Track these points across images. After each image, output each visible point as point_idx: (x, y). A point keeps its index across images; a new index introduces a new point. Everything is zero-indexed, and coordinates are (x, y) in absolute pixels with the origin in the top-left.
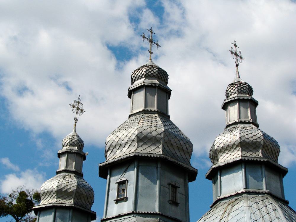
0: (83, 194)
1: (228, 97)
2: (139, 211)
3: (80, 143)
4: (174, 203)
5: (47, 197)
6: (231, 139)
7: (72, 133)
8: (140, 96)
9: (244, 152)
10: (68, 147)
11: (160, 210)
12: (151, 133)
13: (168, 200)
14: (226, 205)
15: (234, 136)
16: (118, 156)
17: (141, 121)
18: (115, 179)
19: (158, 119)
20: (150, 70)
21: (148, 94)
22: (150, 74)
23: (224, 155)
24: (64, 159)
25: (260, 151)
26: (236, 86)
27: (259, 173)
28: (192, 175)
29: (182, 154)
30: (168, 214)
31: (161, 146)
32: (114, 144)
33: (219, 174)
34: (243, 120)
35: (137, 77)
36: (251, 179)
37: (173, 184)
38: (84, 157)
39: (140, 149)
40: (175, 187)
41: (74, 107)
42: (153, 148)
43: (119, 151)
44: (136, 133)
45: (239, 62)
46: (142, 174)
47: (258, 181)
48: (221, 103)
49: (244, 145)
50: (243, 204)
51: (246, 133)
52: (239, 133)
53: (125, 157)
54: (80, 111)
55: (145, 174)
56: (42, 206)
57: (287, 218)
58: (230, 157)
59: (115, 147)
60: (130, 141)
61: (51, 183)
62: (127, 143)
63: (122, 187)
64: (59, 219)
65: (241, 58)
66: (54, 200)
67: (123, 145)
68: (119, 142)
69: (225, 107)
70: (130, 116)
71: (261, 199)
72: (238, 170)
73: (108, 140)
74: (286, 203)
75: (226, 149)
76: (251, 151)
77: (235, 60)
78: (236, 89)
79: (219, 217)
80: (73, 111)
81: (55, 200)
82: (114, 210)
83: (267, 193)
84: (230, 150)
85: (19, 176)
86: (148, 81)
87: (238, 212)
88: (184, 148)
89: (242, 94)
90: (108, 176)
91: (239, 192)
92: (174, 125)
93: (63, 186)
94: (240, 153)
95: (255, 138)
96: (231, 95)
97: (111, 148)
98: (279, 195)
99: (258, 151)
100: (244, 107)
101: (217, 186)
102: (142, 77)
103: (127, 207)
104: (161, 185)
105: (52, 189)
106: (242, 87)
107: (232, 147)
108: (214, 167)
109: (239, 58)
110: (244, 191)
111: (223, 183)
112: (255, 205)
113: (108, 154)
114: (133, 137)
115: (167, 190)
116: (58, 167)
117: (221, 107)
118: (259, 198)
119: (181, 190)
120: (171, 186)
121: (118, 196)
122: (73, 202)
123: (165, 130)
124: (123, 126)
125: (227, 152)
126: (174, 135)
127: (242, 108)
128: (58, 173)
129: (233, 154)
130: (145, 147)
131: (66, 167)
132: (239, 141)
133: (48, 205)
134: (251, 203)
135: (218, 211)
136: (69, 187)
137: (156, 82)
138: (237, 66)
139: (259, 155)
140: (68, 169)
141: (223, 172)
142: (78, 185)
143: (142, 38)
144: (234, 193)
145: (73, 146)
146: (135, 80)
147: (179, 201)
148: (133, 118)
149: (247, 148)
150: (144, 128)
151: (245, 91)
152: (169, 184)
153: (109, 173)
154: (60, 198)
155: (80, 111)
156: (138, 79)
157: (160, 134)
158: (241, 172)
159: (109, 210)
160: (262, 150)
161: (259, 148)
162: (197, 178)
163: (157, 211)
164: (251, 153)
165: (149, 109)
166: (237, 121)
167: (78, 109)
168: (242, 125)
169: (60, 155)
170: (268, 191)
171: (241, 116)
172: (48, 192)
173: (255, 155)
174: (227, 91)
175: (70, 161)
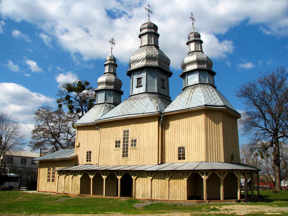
0: (117, 83)
1: (189, 39)
2: (148, 91)
3: (114, 59)
4: (163, 88)
5: (101, 85)
7: (110, 55)
8: (145, 38)
9: (198, 65)
11: (157, 91)
12: (152, 55)
13: (160, 86)
14: (191, 89)
15: (193, 58)
16: (136, 66)
18: (135, 77)
19: (155, 48)
21: (149, 37)
23: (189, 66)
24: (107, 67)
25: (206, 64)
26: (193, 34)
27: (205, 75)
28: (170, 74)
29: (166, 65)
30: (161, 93)
31: (157, 61)
32: (134, 60)
33: (186, 75)
34: (197, 50)
35: (144, 28)
36: (201, 77)
37: (163, 79)
38: (116, 66)
40: (163, 80)
41: (111, 42)
43: (137, 64)
44: (145, 55)
46: (149, 74)
47: (205, 78)
49: (198, 62)
50: (199, 89)
51: (199, 56)
52: (196, 56)
53: (141, 67)
55: (150, 75)
56: (99, 89)
58: (193, 67)
61: (103, 78)
62: (141, 60)
63: (139, 81)
64: (108, 94)
65: (195, 21)
66: (105, 86)
67: (139, 61)
68: (137, 59)
69: (188, 44)
70: (140, 47)
72: (196, 73)
73: (131, 59)
75: (190, 64)
76: (201, 65)
77: (192, 21)
78: (193, 36)
82: (136, 91)
83: (208, 84)
84: (192, 64)
85: (65, 75)
86: (149, 30)
87: (197, 92)
88: (167, 62)
89: (196, 38)
90: (132, 75)
91: (197, 83)
92: (161, 51)
93: (108, 79)
94: (196, 65)
95: (203, 58)
96: (191, 38)
97: (133, 62)
98: (213, 84)
99: (204, 65)
100: (197, 44)
101: (185, 81)
102: (146, 28)
103: (142, 90)
104: (157, 80)
109: (194, 21)
110: (199, 83)
111: (188, 79)
112: (204, 89)
114: (144, 57)
115: (160, 81)
116: (104, 71)
117: (186, 44)
118: (206, 86)
119: (165, 82)
121: (137, 85)
122: (113, 87)
123: (159, 54)
124: (138, 52)
126: (162, 56)
127: (196, 44)
128: (105, 73)
130: (150, 62)
131: (109, 71)
132: (196, 60)
133: (101, 89)
134: (203, 88)
135: (187, 92)
136: (111, 80)
137: (153, 31)
138: (193, 24)
139: (205, 66)
141: (188, 74)
142: (115, 79)
143: (145, 9)
144: (194, 84)
145: (112, 61)
146: (142, 30)
147: (165, 87)
148: (142, 48)
149: (200, 63)
150: (149, 53)
152: (161, 79)
153: (132, 74)
154: (107, 85)
156: (144, 29)
157: (157, 56)
158: (197, 74)
159: (133, 91)
160: (158, 62)
161: (205, 63)
163: (156, 91)
164: (201, 65)
165: (150, 44)
166: (194, 50)
167: (112, 43)
168: (197, 53)
169: (105, 65)
170: (209, 83)
171: (196, 48)
173: (203, 66)
175: (110, 68)
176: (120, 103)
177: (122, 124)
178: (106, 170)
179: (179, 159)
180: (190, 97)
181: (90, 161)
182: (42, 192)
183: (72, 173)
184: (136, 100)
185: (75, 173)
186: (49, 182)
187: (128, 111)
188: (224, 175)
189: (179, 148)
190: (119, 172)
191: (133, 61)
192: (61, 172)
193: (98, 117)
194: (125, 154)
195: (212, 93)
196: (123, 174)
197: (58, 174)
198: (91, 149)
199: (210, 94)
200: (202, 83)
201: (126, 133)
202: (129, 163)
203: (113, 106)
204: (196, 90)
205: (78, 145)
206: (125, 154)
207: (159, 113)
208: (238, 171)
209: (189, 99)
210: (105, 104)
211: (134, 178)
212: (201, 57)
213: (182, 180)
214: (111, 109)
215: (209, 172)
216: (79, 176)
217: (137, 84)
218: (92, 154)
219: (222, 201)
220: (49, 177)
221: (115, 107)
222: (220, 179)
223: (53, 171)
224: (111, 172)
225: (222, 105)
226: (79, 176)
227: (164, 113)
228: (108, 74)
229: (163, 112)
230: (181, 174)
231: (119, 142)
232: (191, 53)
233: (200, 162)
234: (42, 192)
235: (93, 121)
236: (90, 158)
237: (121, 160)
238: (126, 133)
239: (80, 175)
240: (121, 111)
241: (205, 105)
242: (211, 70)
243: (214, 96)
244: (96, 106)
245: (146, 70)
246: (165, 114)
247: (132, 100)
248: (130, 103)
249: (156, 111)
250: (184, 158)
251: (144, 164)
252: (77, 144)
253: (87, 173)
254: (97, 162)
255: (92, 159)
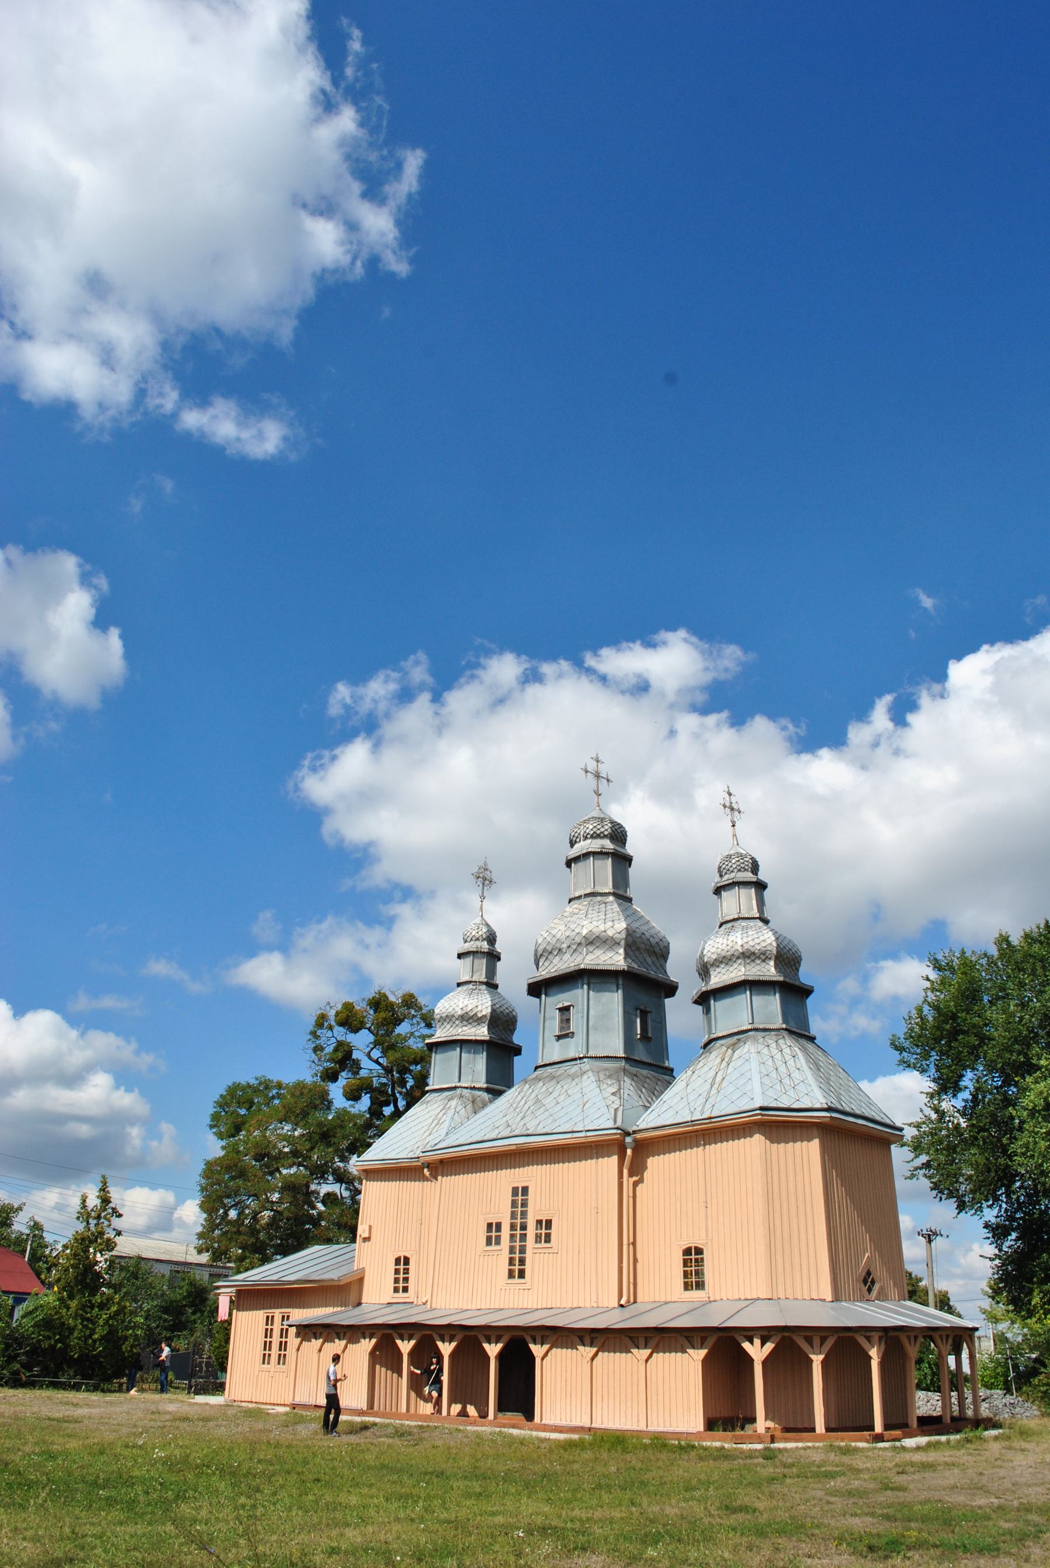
2: (591, 1053)
6: (729, 947)
10: (472, 943)
11: (625, 1052)
14: (724, 1048)
17: (590, 912)
19: (616, 905)
20: (599, 827)
22: (598, 832)
28: (671, 989)
29: (654, 959)
37: (642, 1007)
39: (590, 957)
42: (610, 954)
43: (556, 960)
45: (736, 820)
48: (712, 886)
54: (487, 882)
56: (439, 1040)
57: (812, 1066)
59: (551, 953)
60: (574, 944)
68: (558, 945)
71: (775, 1038)
74: (812, 1039)
75: (721, 962)
79: (714, 1068)
80: (479, 883)
81: (460, 1030)
82: (555, 1051)
83: (783, 1029)
87: (742, 1061)
95: (764, 944)
102: (586, 838)
105: (453, 1013)
106: (742, 861)
107: (730, 960)
108: (704, 989)
109: (736, 813)
112: (765, 1051)
113: (541, 964)
117: (711, 892)
118: (771, 1039)
120: (638, 1011)
123: (628, 925)
125: (722, 966)
129: (731, 969)
134: (760, 1047)
135: (714, 1058)
136: (479, 1008)
138: (733, 826)
140: (475, 978)
141: (718, 996)
144: (736, 1030)
146: (576, 842)
151: (746, 867)
155: (487, 882)
158: (744, 996)
162: (677, 994)
163: (621, 1053)
170: (784, 1026)
172: (447, 1016)
174: (720, 868)
176: (510, 1085)
177: (509, 1162)
178: (449, 1326)
179: (687, 1287)
180: (719, 1078)
181: (405, 1290)
182: (270, 1404)
183: (318, 1335)
184: (554, 1082)
185: (352, 1333)
186: (266, 1366)
187: (526, 1120)
188: (821, 1345)
189: (687, 1252)
190: (491, 1332)
191: (545, 950)
192: (307, 1331)
193: (431, 1141)
194: (517, 1270)
195: (791, 1062)
196: (506, 1338)
197: (298, 1335)
198: (408, 1249)
199: (782, 1069)
200: (761, 1026)
201: (521, 1193)
202: (529, 1301)
203: (486, 1096)
204: (737, 1053)
205: (366, 1235)
206: (517, 1270)
207: (619, 1131)
208: (873, 1334)
209: (716, 1086)
210: (459, 1091)
211: (537, 1350)
212: (757, 941)
213: (624, 1354)
214: (477, 1107)
215: (771, 1336)
216: (367, 1345)
217: (561, 1029)
218: (412, 1266)
219: (820, 1438)
220: (267, 1346)
221: (491, 1101)
222: (812, 1361)
223: (282, 1325)
224: (722, 1334)
225: (818, 1106)
226: (367, 1345)
227: (635, 1132)
228: (471, 986)
229: (635, 1128)
230: (627, 1341)
231: (499, 1226)
232: (729, 925)
233: (746, 1299)
234: (270, 1404)
235: (418, 1153)
236: (406, 1280)
237: (504, 1288)
238: (521, 1193)
239: (367, 1340)
240: (505, 1119)
241: (762, 1109)
242: (797, 983)
243: (796, 1075)
244: (428, 1099)
245: (586, 982)
246: (638, 1136)
247: (541, 1084)
248: (536, 1092)
249: (611, 1124)
250: (700, 1285)
251: (575, 1306)
252: (362, 1230)
253: (390, 1335)
254: (428, 1297)
255: (411, 1284)
